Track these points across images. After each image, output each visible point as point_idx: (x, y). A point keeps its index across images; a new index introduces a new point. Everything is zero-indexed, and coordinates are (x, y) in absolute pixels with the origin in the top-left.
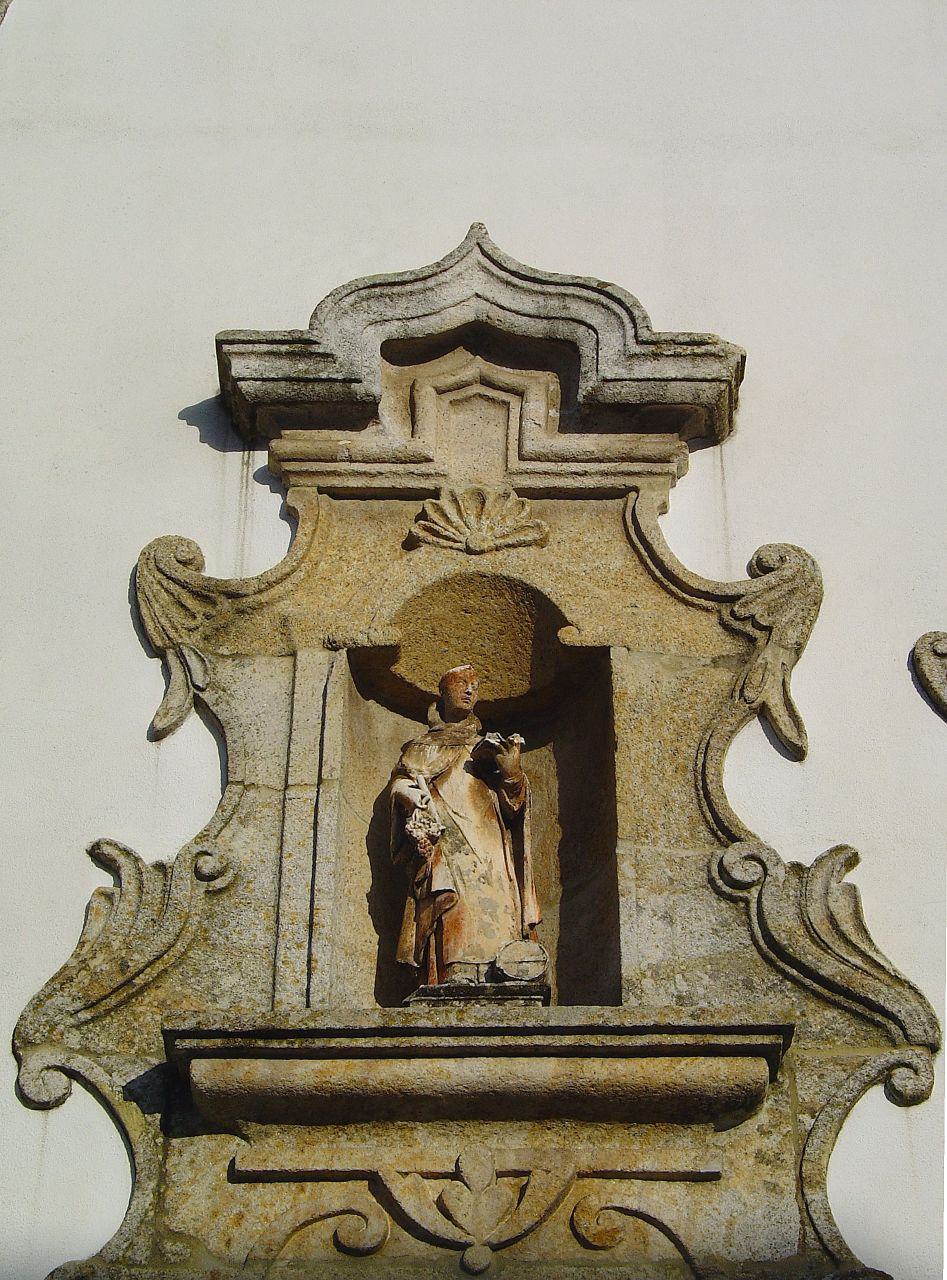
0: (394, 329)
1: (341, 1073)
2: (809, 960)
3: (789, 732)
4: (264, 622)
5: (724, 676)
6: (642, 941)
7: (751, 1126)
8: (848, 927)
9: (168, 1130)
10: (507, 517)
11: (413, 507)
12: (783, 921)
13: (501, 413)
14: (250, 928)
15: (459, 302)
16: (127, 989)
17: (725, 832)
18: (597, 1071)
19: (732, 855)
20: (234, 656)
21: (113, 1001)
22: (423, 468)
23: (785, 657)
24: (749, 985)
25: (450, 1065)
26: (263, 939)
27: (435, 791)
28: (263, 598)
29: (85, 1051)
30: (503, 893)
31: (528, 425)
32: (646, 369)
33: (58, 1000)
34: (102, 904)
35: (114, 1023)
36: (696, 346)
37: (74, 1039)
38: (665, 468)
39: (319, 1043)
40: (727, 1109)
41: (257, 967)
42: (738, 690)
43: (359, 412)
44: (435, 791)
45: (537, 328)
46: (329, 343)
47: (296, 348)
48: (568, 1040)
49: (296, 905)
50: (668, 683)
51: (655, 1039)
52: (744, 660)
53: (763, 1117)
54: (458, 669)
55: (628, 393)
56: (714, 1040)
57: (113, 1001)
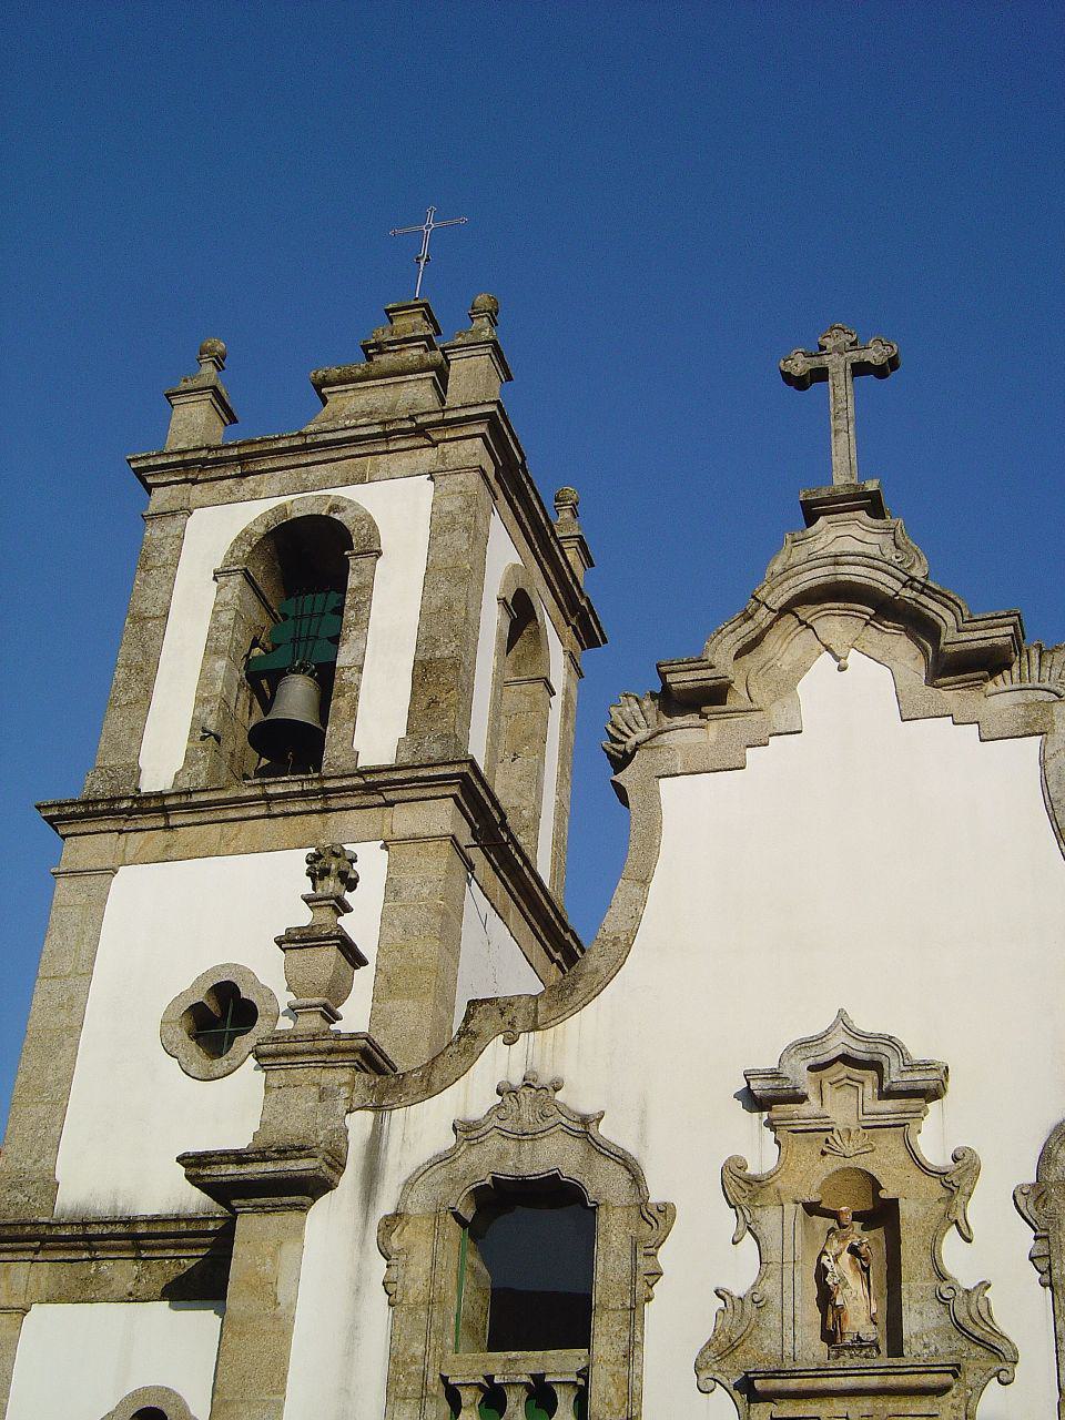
0: (811, 1061)
1: (806, 1384)
2: (970, 1330)
3: (965, 1232)
4: (771, 1190)
5: (942, 1206)
6: (911, 1324)
7: (950, 1394)
8: (985, 1315)
9: (749, 1401)
10: (859, 1140)
11: (824, 1135)
12: (961, 1314)
13: (853, 1091)
14: (773, 1320)
15: (835, 1046)
16: (733, 1347)
17: (942, 1277)
18: (892, 1381)
19: (943, 1287)
20: (761, 1206)
21: (728, 1352)
22: (827, 1120)
23: (964, 1199)
24: (950, 1339)
25: (841, 1379)
26: (778, 1325)
27: (836, 1261)
28: (769, 1181)
29: (719, 1371)
30: (863, 1304)
31: (865, 1099)
32: (908, 1077)
33: (708, 1353)
34: (720, 1314)
35: (728, 1360)
36: (926, 1066)
37: (715, 1367)
38: (919, 1114)
39: (797, 1374)
40: (942, 1390)
41: (776, 1337)
42: (947, 1214)
43: (802, 1099)
44: (836, 1261)
45: (866, 1057)
46: (786, 1072)
47: (774, 1076)
48: (882, 1371)
49: (788, 1312)
50: (922, 1210)
51: (912, 1369)
52: (950, 1199)
53: (954, 1391)
54: (843, 1209)
55: (902, 1087)
56: (932, 1369)
57: (728, 1352)
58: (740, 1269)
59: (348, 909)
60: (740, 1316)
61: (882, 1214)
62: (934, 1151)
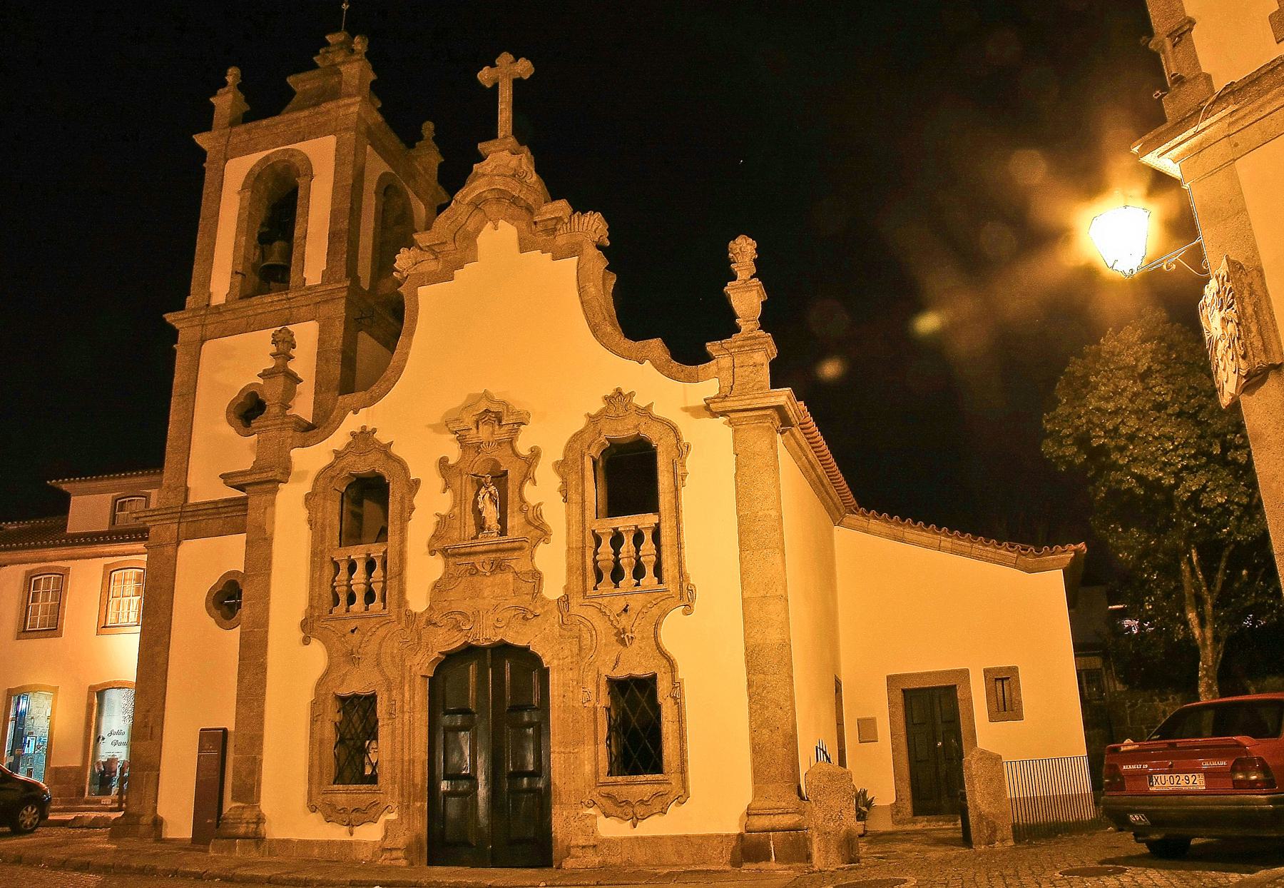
58: (444, 503)
59: (292, 358)
60: (443, 522)
61: (500, 478)
62: (523, 447)
